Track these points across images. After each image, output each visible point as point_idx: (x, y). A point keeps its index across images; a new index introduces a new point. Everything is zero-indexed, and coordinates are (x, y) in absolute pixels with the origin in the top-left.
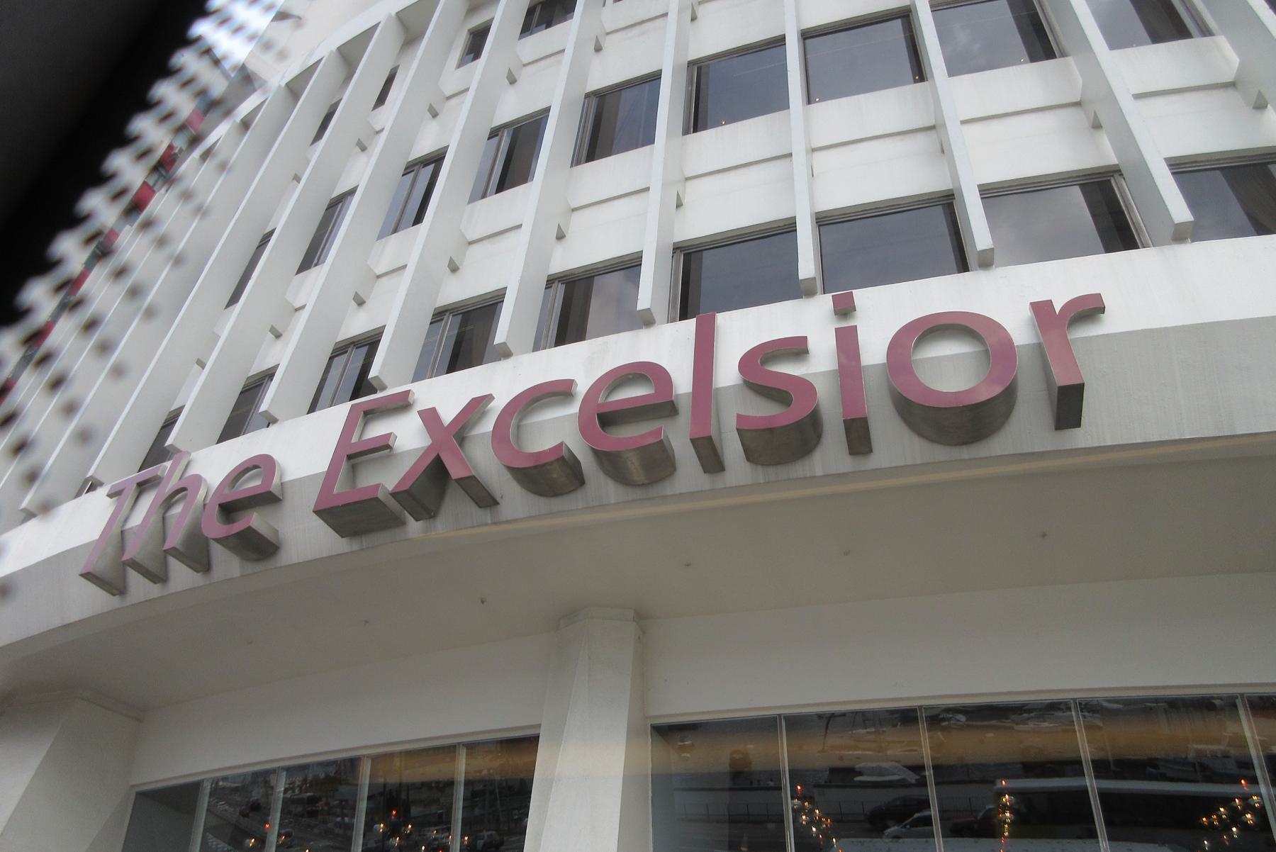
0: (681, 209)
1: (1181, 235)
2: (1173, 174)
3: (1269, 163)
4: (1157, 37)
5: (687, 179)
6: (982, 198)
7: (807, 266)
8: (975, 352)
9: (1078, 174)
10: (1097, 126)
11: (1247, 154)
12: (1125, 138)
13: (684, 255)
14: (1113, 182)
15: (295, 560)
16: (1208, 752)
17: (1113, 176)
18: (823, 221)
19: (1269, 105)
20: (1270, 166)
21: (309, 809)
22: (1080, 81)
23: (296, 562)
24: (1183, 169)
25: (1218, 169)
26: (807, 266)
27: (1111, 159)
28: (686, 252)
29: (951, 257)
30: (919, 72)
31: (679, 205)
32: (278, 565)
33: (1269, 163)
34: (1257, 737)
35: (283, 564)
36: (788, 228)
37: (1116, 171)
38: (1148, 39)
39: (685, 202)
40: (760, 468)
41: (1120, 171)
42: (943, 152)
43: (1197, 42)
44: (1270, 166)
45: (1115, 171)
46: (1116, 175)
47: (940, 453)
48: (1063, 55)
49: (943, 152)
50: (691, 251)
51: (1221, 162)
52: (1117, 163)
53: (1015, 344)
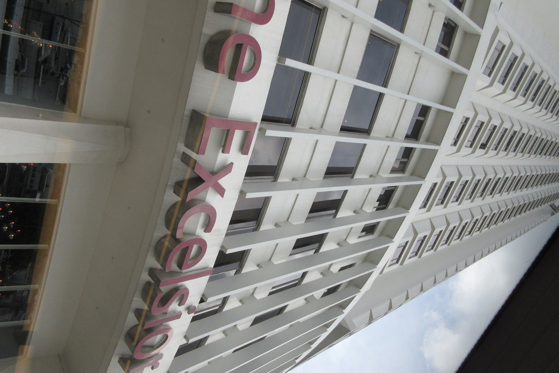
0: (341, 16)
1: (242, 193)
2: (266, 197)
3: (257, 221)
4: (328, 168)
5: (352, 24)
6: (286, 138)
7: (290, 63)
8: (215, 166)
9: (297, 117)
10: (293, 179)
11: (263, 215)
12: (285, 187)
13: (321, 9)
14: (272, 177)
15: (195, 73)
16: (37, 286)
17: (274, 178)
18: (306, 76)
19: (275, 228)
20: (256, 221)
21: (59, 71)
22: (312, 179)
23: (194, 74)
24: (267, 200)
25: (292, 118)
26: (290, 63)
27: (280, 180)
28: (322, 11)
29: (270, 115)
30: (344, 129)
31: (343, 16)
32: (197, 62)
33: (257, 221)
34: (19, 290)
35: (196, 65)
36: (310, 61)
37: (275, 180)
38: (331, 166)
39: (344, 19)
40: (174, 184)
41: (275, 182)
42: (311, 128)
43: (306, 214)
44: (256, 221)
45: (275, 179)
46: (274, 179)
47: (204, 41)
48: (324, 178)
49: (311, 128)
50: (322, 12)
51: (300, 100)
52: (278, 181)
53: (238, 82)
